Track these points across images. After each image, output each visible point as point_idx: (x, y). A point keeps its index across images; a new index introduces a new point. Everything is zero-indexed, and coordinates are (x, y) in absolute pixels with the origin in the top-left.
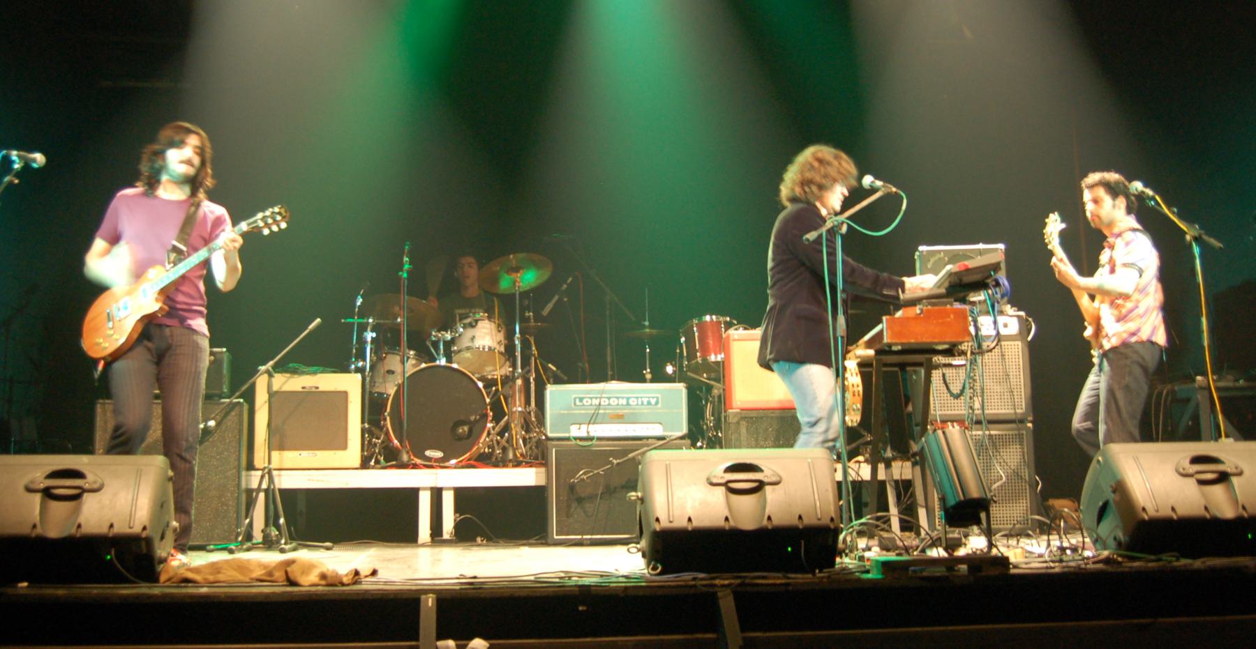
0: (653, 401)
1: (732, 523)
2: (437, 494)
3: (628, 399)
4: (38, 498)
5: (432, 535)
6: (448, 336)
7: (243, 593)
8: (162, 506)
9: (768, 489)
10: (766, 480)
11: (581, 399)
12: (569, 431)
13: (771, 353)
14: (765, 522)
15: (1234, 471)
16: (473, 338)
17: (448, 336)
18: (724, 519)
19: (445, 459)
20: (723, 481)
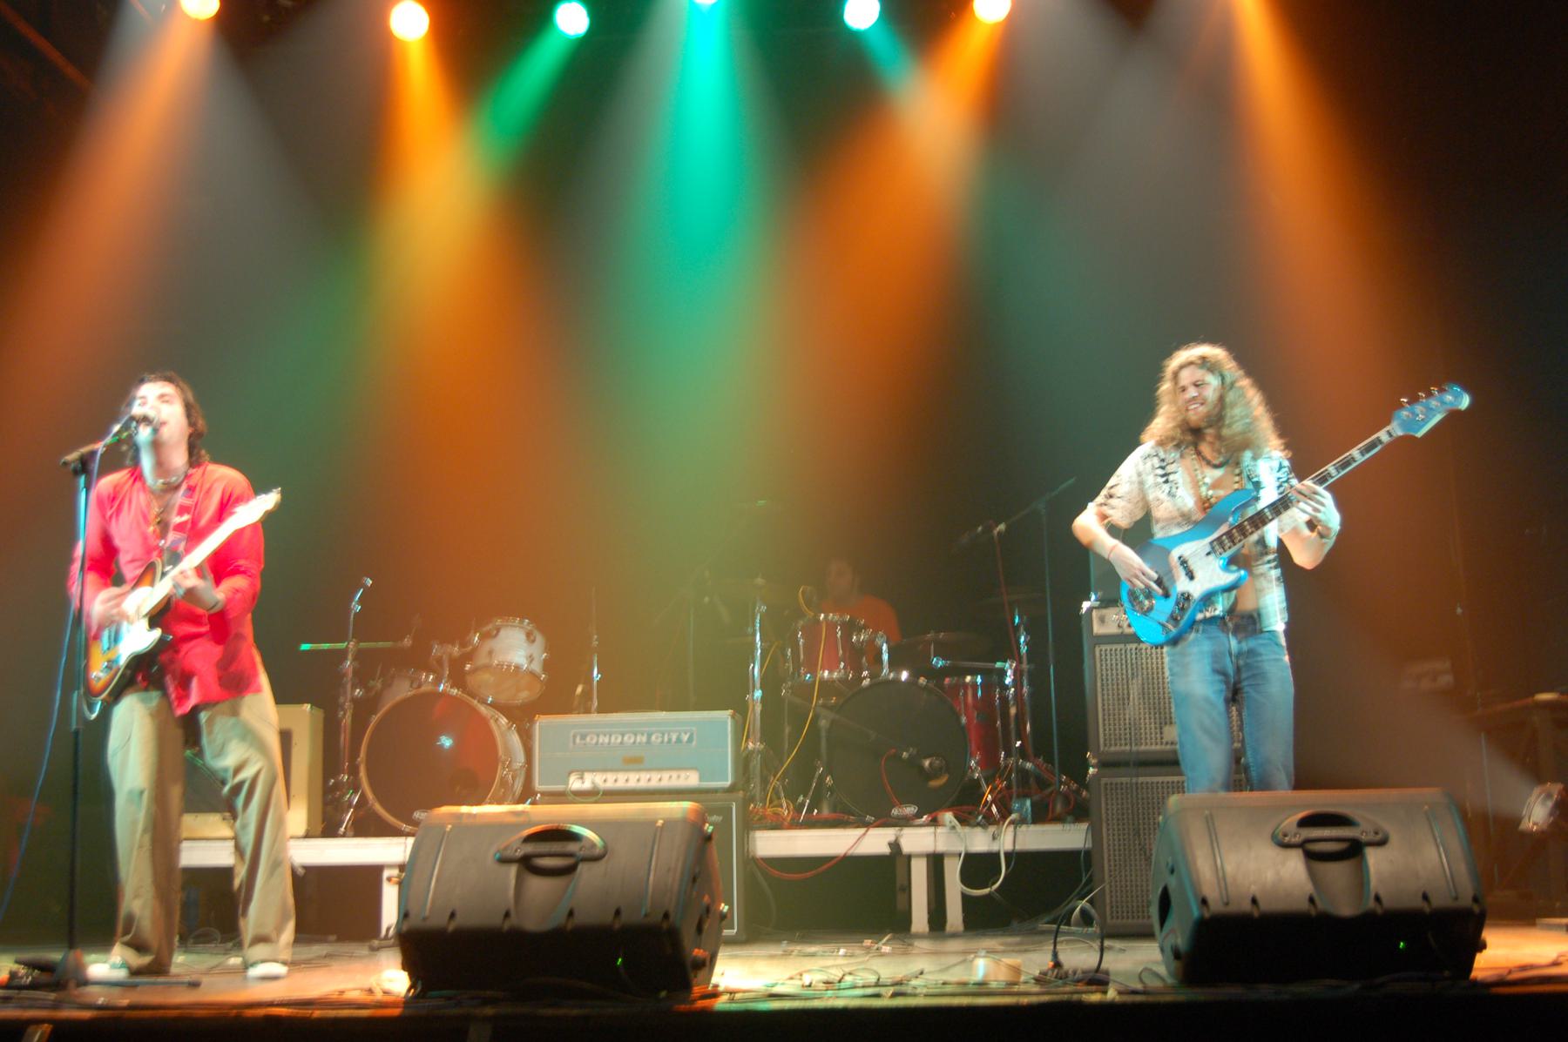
0: (685, 738)
1: (513, 921)
2: (936, 862)
3: (649, 736)
4: (513, 870)
5: (930, 921)
6: (456, 650)
7: (280, 1014)
8: (694, 880)
9: (582, 867)
10: (1364, 838)
11: (583, 737)
12: (567, 783)
13: (789, 667)
14: (1371, 904)
15: (1371, 837)
16: (490, 653)
17: (456, 650)
18: (613, 913)
19: (919, 815)
20: (1297, 840)
